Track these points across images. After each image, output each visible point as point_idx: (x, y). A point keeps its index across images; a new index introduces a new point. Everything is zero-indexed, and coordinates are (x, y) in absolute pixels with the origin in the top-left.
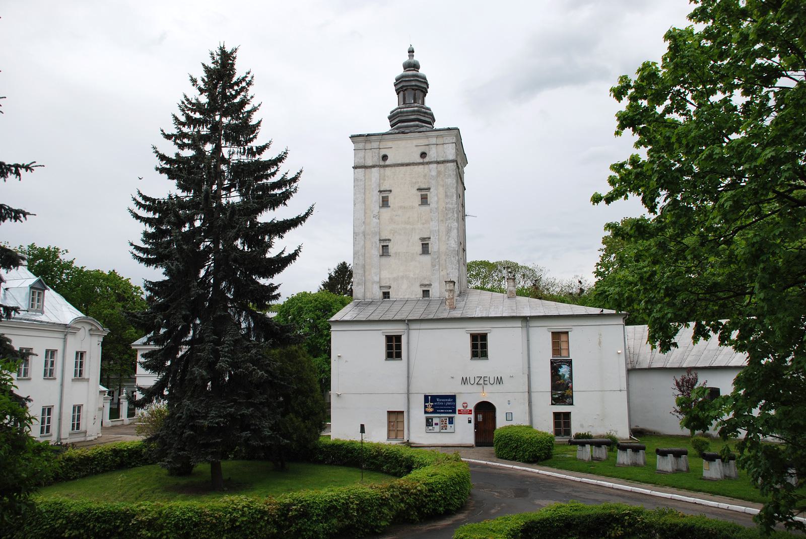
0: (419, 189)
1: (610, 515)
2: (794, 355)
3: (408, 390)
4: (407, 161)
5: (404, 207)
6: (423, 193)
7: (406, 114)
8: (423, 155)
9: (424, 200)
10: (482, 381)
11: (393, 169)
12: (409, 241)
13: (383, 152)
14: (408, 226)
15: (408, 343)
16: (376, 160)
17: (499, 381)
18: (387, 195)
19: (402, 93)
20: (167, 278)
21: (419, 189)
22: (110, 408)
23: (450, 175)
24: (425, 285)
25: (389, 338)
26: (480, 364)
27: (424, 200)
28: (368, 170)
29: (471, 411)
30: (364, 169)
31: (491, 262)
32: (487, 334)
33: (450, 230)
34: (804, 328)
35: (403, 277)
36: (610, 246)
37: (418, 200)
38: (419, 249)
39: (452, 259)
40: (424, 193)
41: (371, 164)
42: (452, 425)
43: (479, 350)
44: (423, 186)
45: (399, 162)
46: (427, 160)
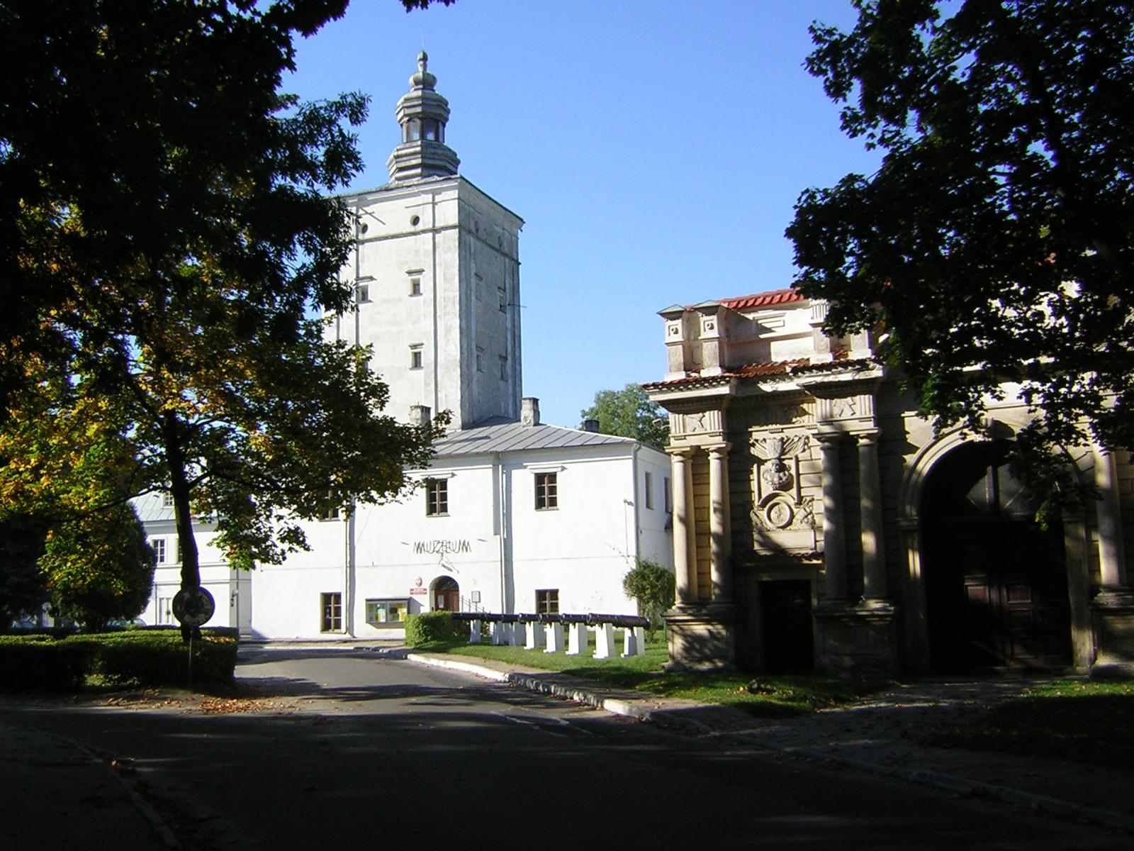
0: (410, 273)
1: (689, 688)
2: (909, 261)
5: (389, 300)
7: (405, 158)
8: (416, 221)
9: (416, 289)
10: (442, 547)
17: (465, 546)
20: (905, 457)
21: (410, 273)
23: (449, 248)
25: (540, 478)
26: (437, 520)
27: (416, 289)
29: (425, 590)
32: (446, 479)
33: (450, 330)
34: (131, 434)
37: (409, 289)
38: (409, 361)
40: (415, 277)
43: (546, 496)
44: (414, 268)
46: (420, 227)
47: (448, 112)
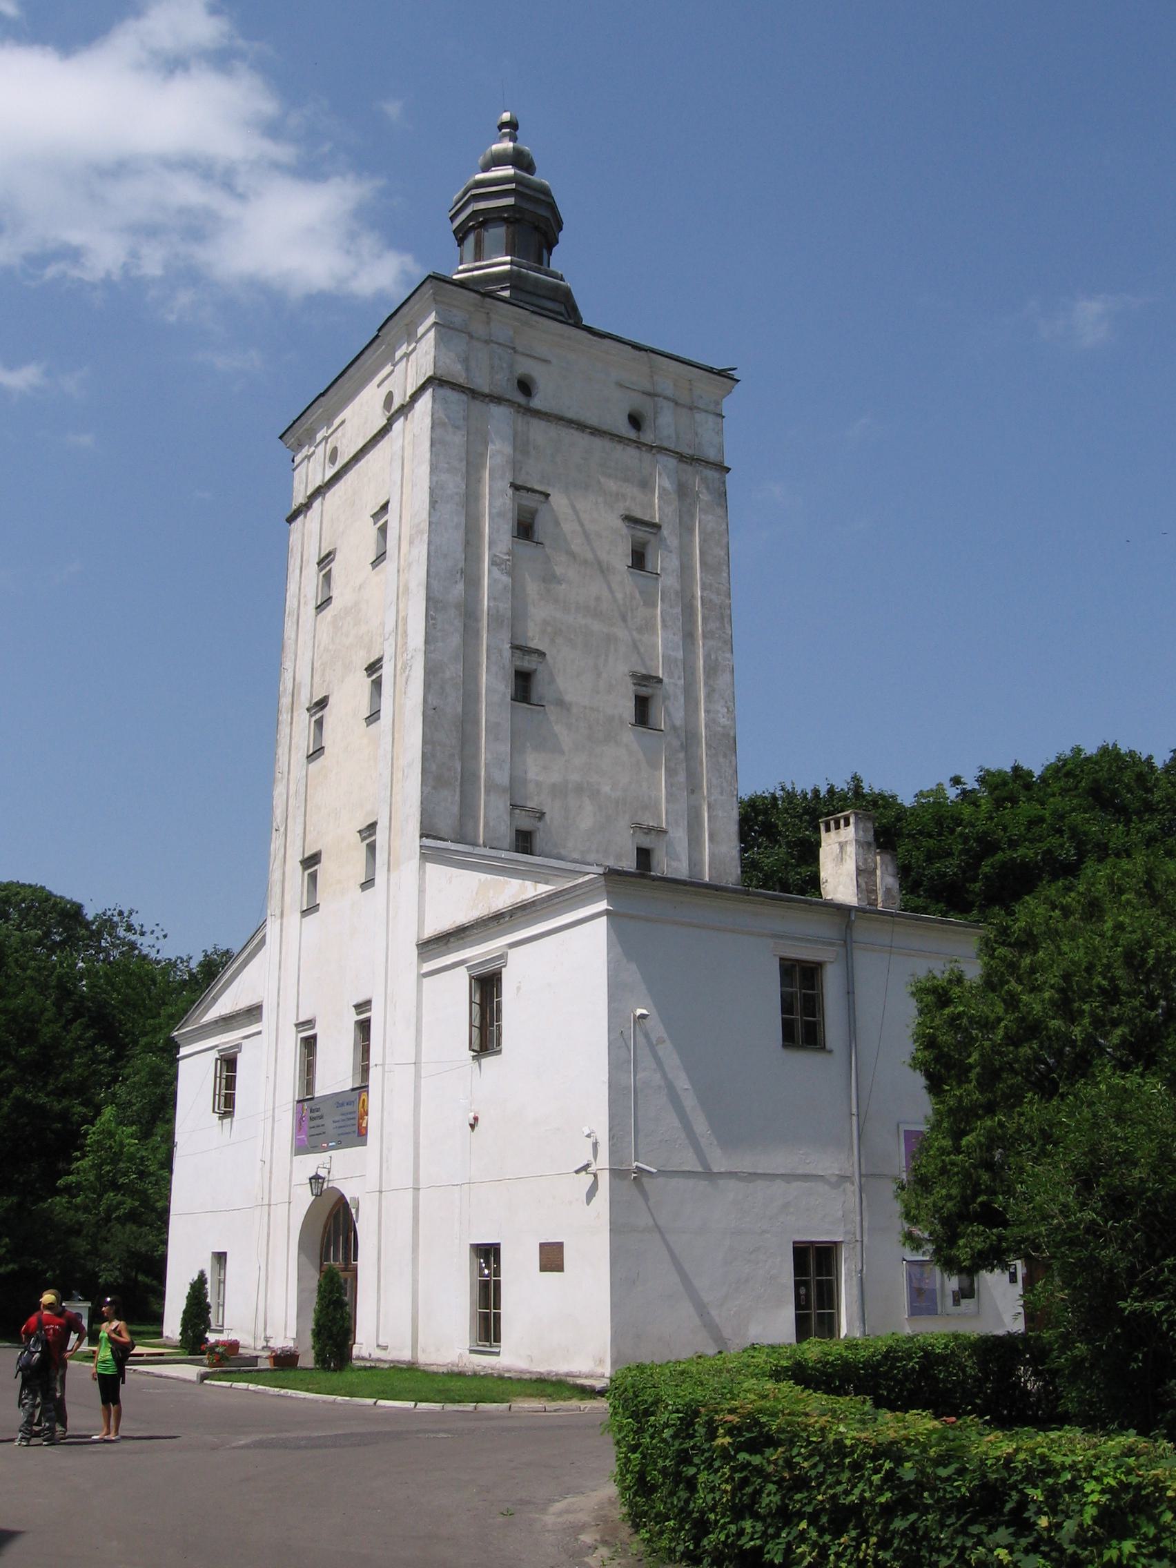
3: (416, 1179)
4: (593, 421)
6: (640, 534)
11: (554, 431)
12: (599, 675)
13: (525, 367)
14: (596, 626)
15: (850, 992)
16: (503, 383)
18: (532, 504)
19: (471, 239)
22: (794, 1247)
24: (649, 830)
28: (477, 405)
30: (464, 397)
31: (1036, 766)
35: (579, 789)
36: (74, 904)
38: (627, 709)
39: (721, 760)
41: (486, 390)
42: (915, 1285)
45: (570, 414)
47: (559, 225)
